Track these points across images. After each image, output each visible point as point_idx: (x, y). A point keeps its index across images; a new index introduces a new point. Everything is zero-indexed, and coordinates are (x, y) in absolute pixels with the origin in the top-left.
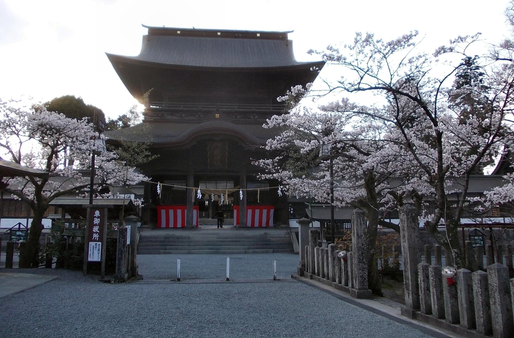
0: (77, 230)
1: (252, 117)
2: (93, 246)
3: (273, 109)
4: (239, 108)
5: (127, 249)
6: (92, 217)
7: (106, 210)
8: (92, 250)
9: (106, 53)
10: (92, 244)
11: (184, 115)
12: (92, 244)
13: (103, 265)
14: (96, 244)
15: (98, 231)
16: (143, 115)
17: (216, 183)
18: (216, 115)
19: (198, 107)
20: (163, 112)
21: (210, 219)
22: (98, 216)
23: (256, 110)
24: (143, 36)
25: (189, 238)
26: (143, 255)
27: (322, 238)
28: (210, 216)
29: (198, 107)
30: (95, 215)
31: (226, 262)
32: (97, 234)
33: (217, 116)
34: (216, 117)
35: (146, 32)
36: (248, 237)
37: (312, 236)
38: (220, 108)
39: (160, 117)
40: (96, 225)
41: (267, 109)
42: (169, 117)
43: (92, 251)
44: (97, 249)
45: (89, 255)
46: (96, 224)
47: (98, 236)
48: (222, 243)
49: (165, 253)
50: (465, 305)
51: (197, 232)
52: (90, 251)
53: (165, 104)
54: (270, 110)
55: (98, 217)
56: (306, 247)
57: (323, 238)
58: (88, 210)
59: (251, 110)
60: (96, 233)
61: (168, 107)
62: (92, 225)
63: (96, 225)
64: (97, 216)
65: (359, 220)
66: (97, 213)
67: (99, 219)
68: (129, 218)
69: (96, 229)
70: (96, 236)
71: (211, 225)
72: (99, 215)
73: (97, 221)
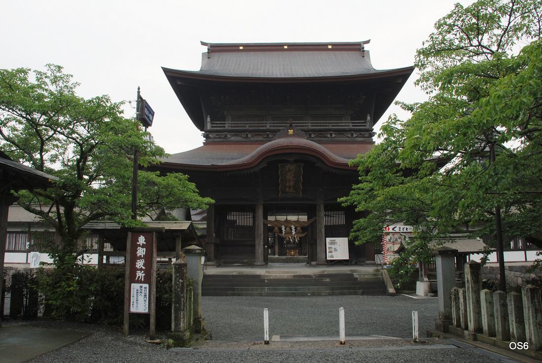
1: (329, 136)
2: (137, 290)
3: (353, 126)
5: (187, 295)
6: (135, 246)
8: (135, 296)
9: (163, 68)
10: (135, 287)
11: (249, 136)
12: (135, 287)
13: (152, 320)
15: (144, 268)
16: (204, 137)
18: (289, 130)
19: (266, 126)
23: (333, 128)
24: (203, 53)
27: (422, 275)
29: (266, 126)
31: (338, 316)
32: (143, 272)
33: (291, 132)
34: (289, 133)
35: (205, 49)
38: (294, 123)
40: (140, 258)
42: (233, 138)
43: (135, 297)
44: (143, 295)
45: (131, 305)
47: (144, 274)
49: (233, 295)
50: (64, 219)
52: (133, 297)
54: (349, 127)
55: (143, 246)
57: (423, 276)
59: (327, 128)
60: (141, 269)
61: (232, 127)
63: (140, 258)
64: (141, 245)
66: (142, 240)
67: (145, 249)
69: (140, 264)
70: (140, 275)
72: (145, 243)
73: (141, 252)
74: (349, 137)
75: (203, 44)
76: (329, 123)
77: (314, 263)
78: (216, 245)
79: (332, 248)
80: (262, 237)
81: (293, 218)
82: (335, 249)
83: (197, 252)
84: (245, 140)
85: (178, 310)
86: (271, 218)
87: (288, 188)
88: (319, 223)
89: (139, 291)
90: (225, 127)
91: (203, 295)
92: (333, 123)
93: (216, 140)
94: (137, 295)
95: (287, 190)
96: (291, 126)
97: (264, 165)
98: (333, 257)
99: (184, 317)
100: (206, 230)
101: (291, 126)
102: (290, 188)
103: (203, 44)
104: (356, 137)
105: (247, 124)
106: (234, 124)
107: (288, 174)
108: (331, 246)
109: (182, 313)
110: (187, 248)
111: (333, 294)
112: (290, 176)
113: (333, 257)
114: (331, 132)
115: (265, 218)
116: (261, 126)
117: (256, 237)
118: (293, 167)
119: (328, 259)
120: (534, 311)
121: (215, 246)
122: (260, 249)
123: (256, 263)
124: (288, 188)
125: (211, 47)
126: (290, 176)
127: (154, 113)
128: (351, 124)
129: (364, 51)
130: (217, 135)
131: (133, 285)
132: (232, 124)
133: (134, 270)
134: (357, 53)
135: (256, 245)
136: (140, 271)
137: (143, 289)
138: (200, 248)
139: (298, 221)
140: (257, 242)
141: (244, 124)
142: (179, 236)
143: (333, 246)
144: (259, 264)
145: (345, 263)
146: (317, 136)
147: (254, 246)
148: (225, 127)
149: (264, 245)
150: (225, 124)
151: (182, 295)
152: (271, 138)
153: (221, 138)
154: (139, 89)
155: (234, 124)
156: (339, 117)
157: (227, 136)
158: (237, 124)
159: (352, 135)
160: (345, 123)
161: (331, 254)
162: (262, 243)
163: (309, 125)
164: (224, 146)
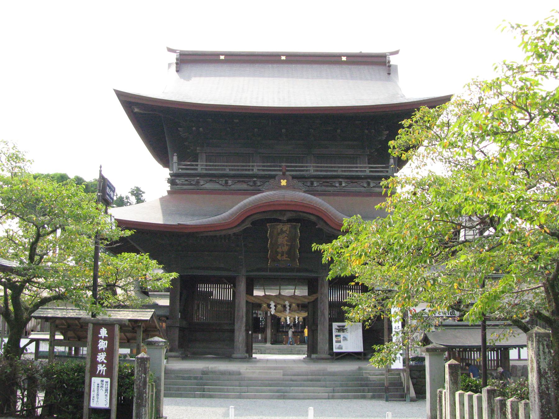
0: (72, 357)
2: (98, 384)
3: (371, 171)
4: (317, 171)
6: (96, 339)
7: (117, 328)
8: (96, 390)
10: (96, 381)
11: (230, 182)
12: (96, 381)
14: (102, 381)
16: (168, 182)
17: (264, 289)
18: (282, 181)
20: (198, 178)
21: (268, 345)
22: (105, 336)
25: (239, 373)
26: (185, 398)
28: (268, 339)
29: (253, 170)
30: (100, 335)
32: (104, 365)
33: (284, 183)
34: (282, 184)
35: (173, 58)
36: (333, 374)
37: (451, 374)
38: (288, 171)
39: (195, 185)
40: (102, 351)
41: (361, 171)
42: (209, 186)
43: (96, 392)
44: (104, 389)
46: (103, 348)
47: (105, 368)
48: (292, 382)
49: (203, 396)
51: (253, 366)
52: (94, 391)
53: (314, 167)
55: (105, 339)
56: (438, 392)
58: (91, 326)
59: (334, 173)
60: (102, 363)
61: (206, 170)
62: (95, 351)
63: (102, 351)
64: (103, 337)
65: (541, 347)
66: (103, 332)
67: (107, 342)
68: (153, 341)
69: (101, 357)
70: (101, 368)
71: (269, 353)
72: (107, 336)
74: (365, 187)
75: (170, 50)
76: (339, 167)
77: (314, 356)
78: (182, 329)
79: (339, 336)
80: (244, 320)
81: (288, 292)
82: (344, 337)
83: (161, 344)
84: (224, 188)
85: (139, 406)
86: (258, 293)
87: (280, 255)
88: (321, 303)
89: (100, 386)
90: (196, 169)
91: (165, 396)
92: (345, 167)
93: (185, 187)
94: (98, 390)
95: (279, 257)
96: (284, 174)
97: (248, 225)
98: (342, 348)
99: (145, 414)
100: (168, 309)
101: (284, 174)
102: (282, 255)
103: (170, 50)
104: (374, 187)
105: (226, 166)
106: (210, 166)
107: (280, 236)
108: (338, 334)
109: (144, 410)
110: (150, 340)
111: (333, 398)
112: (282, 240)
113: (342, 348)
114: (340, 180)
115: (250, 292)
116: (246, 170)
117: (236, 320)
118: (286, 227)
119: (335, 350)
120: (490, 412)
121: (180, 330)
122: (240, 336)
123: (234, 356)
124: (280, 255)
125: (180, 55)
126: (282, 240)
127: (114, 188)
128: (368, 170)
129: (390, 66)
130: (186, 180)
131: (93, 379)
132: (206, 166)
133: (95, 363)
134: (381, 68)
135: (236, 331)
136: (101, 365)
137: (104, 383)
138: (164, 340)
139: (294, 297)
140: (236, 327)
141: (223, 166)
142: (140, 326)
143: (342, 334)
144: (238, 355)
145: (356, 356)
146: (321, 185)
147: (232, 331)
148: (196, 169)
149: (247, 331)
150: (197, 165)
151: (144, 391)
152: (259, 186)
153: (191, 185)
154: (101, 167)
155: (210, 166)
156: (353, 159)
157: (199, 183)
158: (213, 166)
159: (369, 184)
160: (361, 167)
161: (338, 344)
162: (243, 328)
163: (311, 169)
164: (196, 196)
